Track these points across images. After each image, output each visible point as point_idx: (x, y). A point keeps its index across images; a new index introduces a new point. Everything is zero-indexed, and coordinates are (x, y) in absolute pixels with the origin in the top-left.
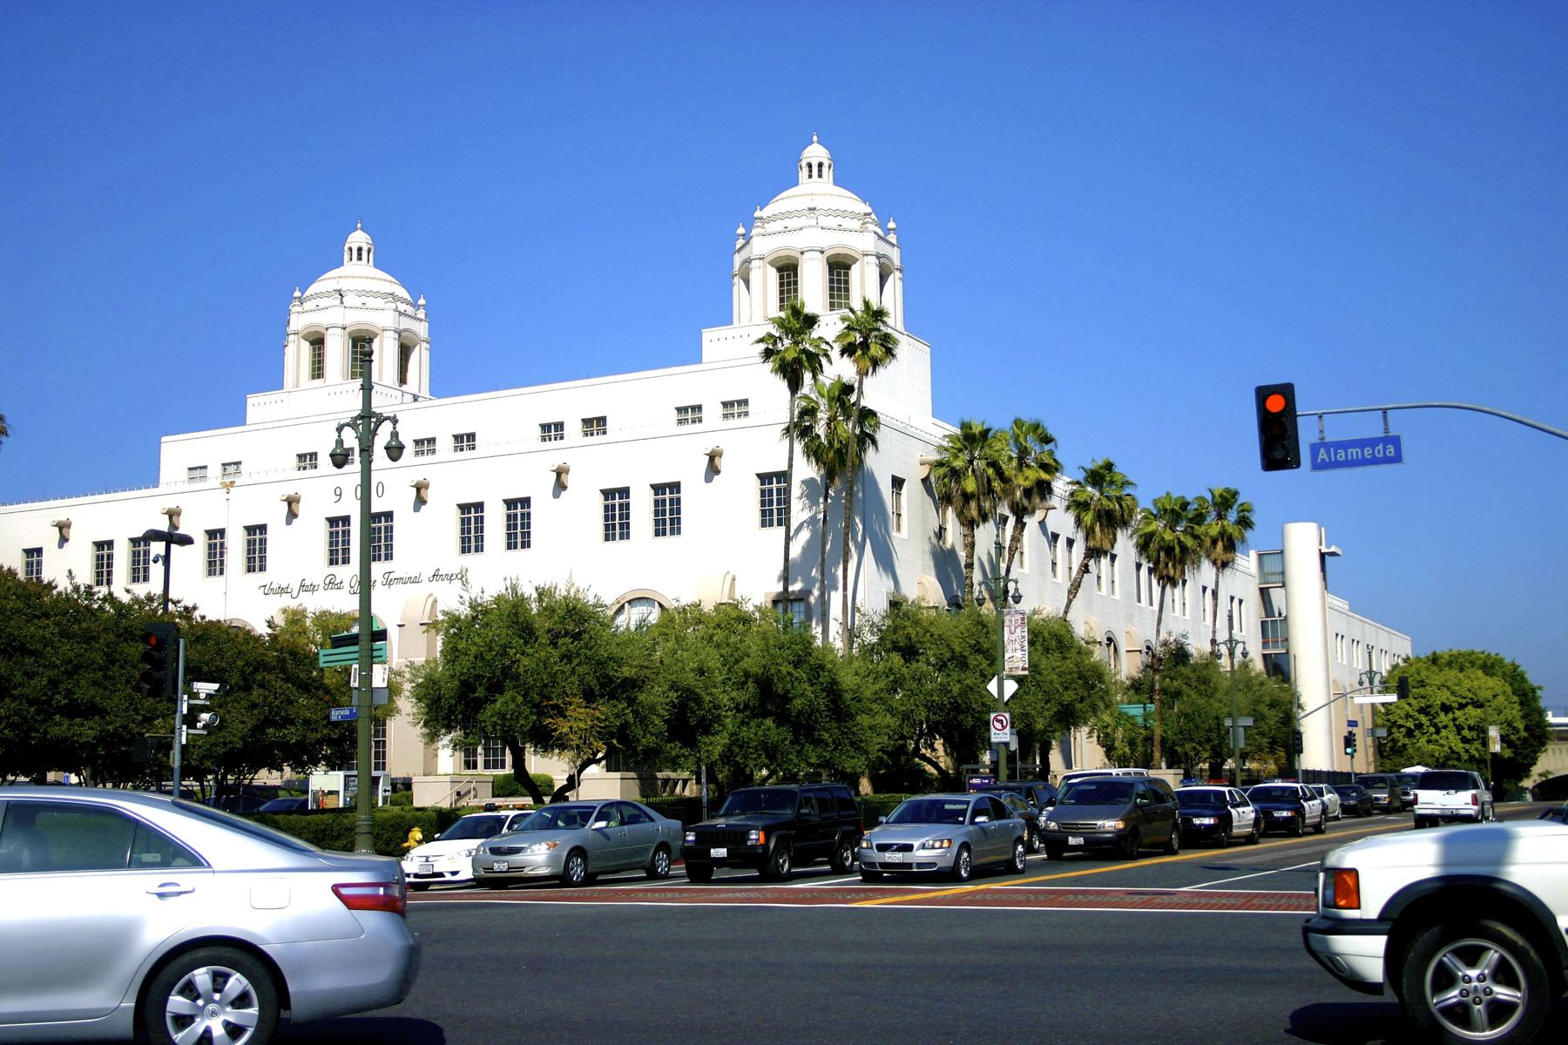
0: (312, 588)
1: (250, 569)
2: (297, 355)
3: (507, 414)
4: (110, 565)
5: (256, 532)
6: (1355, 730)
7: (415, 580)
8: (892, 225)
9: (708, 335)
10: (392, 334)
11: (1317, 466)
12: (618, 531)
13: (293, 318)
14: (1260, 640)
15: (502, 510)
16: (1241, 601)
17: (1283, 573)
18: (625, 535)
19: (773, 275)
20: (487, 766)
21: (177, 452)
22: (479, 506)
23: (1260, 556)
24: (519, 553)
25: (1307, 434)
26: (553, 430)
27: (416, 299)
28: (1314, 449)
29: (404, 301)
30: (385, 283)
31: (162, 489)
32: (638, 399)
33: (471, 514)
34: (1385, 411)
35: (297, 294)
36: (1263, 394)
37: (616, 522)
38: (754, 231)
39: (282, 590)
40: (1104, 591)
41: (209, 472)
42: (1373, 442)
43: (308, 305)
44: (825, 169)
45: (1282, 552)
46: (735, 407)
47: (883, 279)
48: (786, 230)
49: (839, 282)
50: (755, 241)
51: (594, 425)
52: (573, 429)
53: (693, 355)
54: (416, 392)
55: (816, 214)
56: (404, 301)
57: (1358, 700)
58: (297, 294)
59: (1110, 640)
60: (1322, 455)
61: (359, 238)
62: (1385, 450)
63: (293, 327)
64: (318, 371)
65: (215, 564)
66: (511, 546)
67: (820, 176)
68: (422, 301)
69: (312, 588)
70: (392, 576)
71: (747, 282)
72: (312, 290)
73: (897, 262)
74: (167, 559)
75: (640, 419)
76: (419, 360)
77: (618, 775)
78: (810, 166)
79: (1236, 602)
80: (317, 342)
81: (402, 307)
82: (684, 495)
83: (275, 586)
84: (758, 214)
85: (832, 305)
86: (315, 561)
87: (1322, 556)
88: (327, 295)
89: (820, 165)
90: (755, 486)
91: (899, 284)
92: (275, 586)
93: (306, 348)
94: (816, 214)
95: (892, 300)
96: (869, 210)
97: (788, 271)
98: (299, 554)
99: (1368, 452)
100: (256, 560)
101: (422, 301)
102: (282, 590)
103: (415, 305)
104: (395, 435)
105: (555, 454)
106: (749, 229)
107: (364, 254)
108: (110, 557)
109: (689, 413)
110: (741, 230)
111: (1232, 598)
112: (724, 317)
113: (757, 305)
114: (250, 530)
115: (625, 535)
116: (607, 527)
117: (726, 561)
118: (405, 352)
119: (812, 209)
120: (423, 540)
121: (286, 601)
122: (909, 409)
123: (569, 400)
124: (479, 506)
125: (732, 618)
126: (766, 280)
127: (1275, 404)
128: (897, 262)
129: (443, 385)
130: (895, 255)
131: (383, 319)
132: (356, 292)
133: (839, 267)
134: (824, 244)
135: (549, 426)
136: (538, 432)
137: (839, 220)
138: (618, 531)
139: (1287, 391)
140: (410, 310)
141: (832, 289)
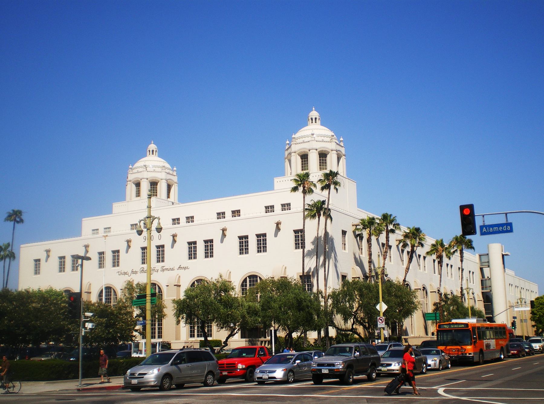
0: (136, 273)
1: (114, 266)
2: (131, 189)
3: (205, 210)
4: (64, 265)
5: (116, 252)
6: (516, 320)
7: (172, 269)
8: (341, 139)
9: (276, 180)
10: (164, 181)
11: (482, 234)
12: (244, 251)
13: (129, 175)
14: (481, 287)
15: (203, 244)
16: (473, 273)
17: (488, 262)
18: (247, 253)
19: (299, 160)
20: (198, 336)
21: (89, 224)
22: (195, 243)
23: (480, 256)
24: (209, 259)
25: (479, 222)
26: (221, 215)
27: (173, 168)
28: (481, 227)
29: (168, 169)
30: (161, 162)
31: (83, 237)
32: (252, 204)
33: (192, 245)
34: (506, 214)
35: (131, 167)
36: (462, 208)
37: (244, 247)
38: (292, 143)
39: (125, 273)
40: (421, 270)
41: (100, 231)
42: (502, 225)
43: (135, 171)
44: (317, 120)
45: (488, 254)
46: (286, 206)
47: (339, 159)
48: (304, 142)
49: (323, 160)
50: (293, 146)
51: (236, 213)
52: (228, 214)
53: (270, 187)
54: (173, 201)
55: (315, 135)
56: (168, 169)
57: (516, 309)
58: (131, 167)
59: (424, 288)
60: (484, 230)
61: (152, 147)
62: (505, 228)
63: (129, 179)
64: (138, 194)
65: (101, 264)
66: (206, 257)
67: (316, 122)
68: (175, 169)
69: (136, 273)
70: (164, 268)
71: (290, 161)
72: (137, 165)
73: (344, 152)
74: (82, 265)
75: (252, 210)
76: (174, 190)
77: (244, 339)
78: (312, 119)
79: (471, 273)
80: (138, 185)
81: (168, 171)
82: (267, 238)
83: (122, 272)
84: (293, 136)
85: (320, 168)
86: (138, 265)
87: (503, 256)
88: (141, 167)
89: (316, 119)
90: (293, 235)
91: (344, 160)
92: (122, 272)
93: (134, 187)
94: (315, 135)
95: (341, 169)
96: (333, 134)
97: (304, 157)
98: (131, 260)
99: (501, 228)
100: (116, 262)
101: (175, 169)
102: (125, 273)
103: (173, 170)
104: (159, 224)
105: (222, 224)
106: (290, 141)
107: (154, 152)
108: (64, 262)
109: (269, 209)
110: (288, 142)
111: (470, 272)
112: (282, 173)
113: (295, 167)
114: (114, 252)
115: (247, 253)
116: (240, 250)
117: (282, 262)
118: (169, 187)
119: (313, 134)
120: (177, 255)
121: (127, 278)
122: (348, 205)
123: (227, 204)
124: (195, 243)
125: (283, 284)
126: (297, 161)
127: (467, 212)
128: (344, 152)
129: (183, 199)
130: (343, 150)
131: (161, 176)
132: (152, 165)
133: (323, 155)
134: (317, 147)
135: (220, 213)
136: (216, 216)
137: (323, 138)
138: (244, 251)
139: (471, 207)
140: (171, 172)
141: (320, 163)
